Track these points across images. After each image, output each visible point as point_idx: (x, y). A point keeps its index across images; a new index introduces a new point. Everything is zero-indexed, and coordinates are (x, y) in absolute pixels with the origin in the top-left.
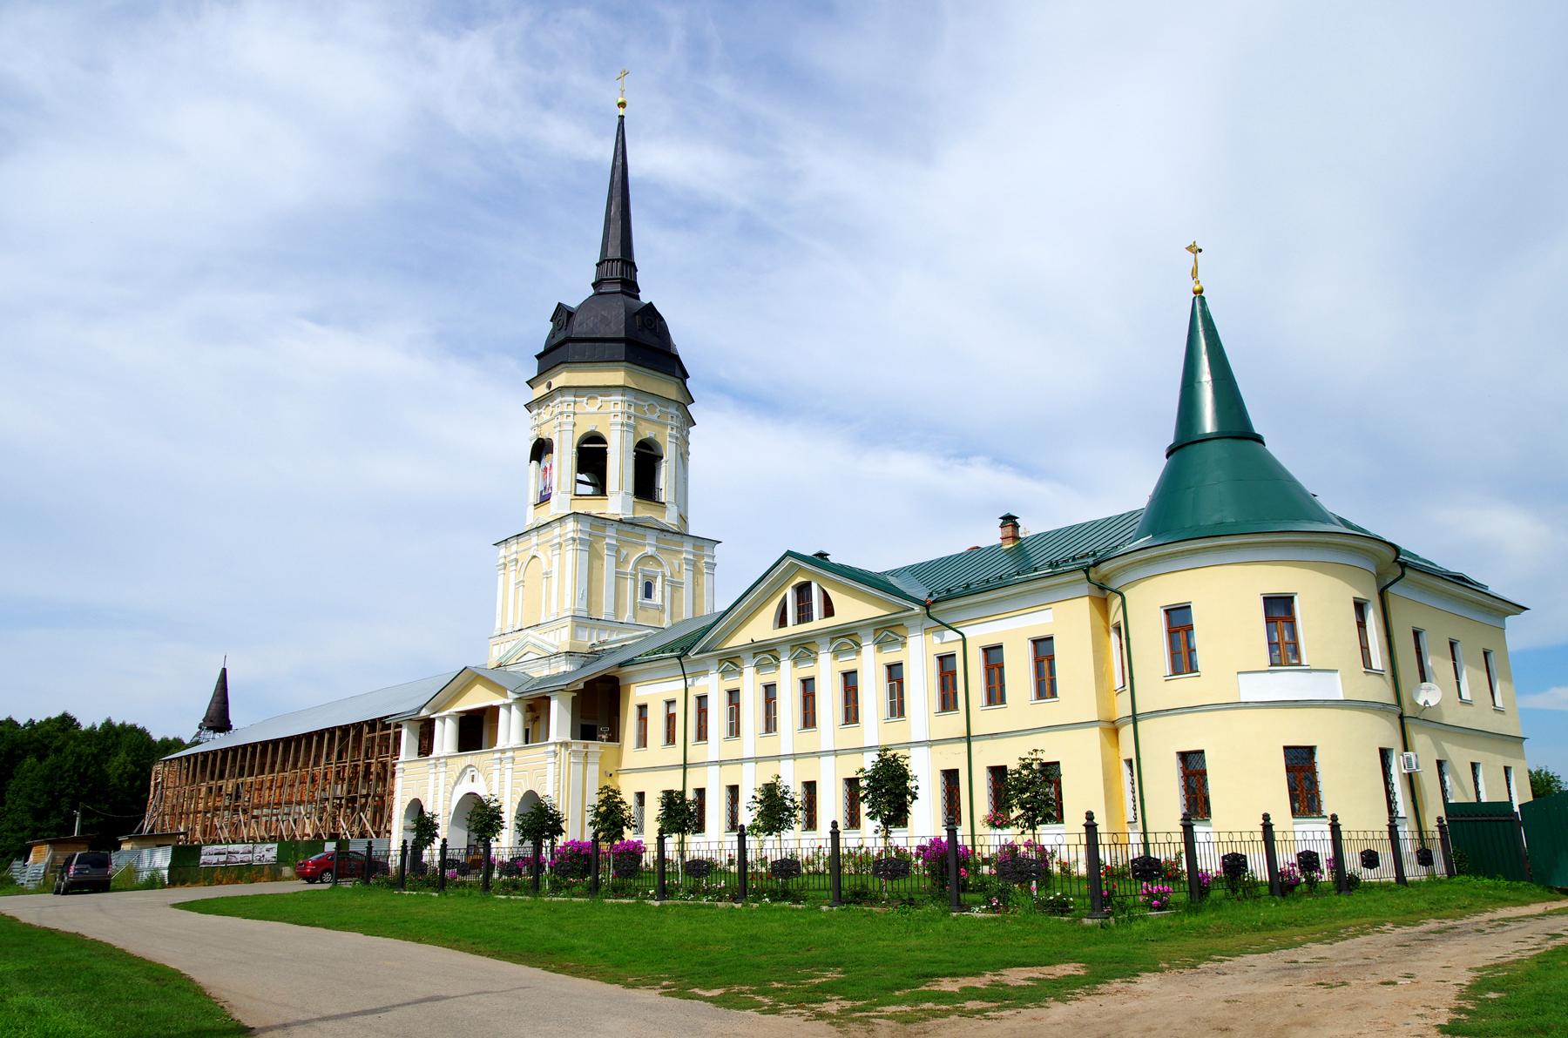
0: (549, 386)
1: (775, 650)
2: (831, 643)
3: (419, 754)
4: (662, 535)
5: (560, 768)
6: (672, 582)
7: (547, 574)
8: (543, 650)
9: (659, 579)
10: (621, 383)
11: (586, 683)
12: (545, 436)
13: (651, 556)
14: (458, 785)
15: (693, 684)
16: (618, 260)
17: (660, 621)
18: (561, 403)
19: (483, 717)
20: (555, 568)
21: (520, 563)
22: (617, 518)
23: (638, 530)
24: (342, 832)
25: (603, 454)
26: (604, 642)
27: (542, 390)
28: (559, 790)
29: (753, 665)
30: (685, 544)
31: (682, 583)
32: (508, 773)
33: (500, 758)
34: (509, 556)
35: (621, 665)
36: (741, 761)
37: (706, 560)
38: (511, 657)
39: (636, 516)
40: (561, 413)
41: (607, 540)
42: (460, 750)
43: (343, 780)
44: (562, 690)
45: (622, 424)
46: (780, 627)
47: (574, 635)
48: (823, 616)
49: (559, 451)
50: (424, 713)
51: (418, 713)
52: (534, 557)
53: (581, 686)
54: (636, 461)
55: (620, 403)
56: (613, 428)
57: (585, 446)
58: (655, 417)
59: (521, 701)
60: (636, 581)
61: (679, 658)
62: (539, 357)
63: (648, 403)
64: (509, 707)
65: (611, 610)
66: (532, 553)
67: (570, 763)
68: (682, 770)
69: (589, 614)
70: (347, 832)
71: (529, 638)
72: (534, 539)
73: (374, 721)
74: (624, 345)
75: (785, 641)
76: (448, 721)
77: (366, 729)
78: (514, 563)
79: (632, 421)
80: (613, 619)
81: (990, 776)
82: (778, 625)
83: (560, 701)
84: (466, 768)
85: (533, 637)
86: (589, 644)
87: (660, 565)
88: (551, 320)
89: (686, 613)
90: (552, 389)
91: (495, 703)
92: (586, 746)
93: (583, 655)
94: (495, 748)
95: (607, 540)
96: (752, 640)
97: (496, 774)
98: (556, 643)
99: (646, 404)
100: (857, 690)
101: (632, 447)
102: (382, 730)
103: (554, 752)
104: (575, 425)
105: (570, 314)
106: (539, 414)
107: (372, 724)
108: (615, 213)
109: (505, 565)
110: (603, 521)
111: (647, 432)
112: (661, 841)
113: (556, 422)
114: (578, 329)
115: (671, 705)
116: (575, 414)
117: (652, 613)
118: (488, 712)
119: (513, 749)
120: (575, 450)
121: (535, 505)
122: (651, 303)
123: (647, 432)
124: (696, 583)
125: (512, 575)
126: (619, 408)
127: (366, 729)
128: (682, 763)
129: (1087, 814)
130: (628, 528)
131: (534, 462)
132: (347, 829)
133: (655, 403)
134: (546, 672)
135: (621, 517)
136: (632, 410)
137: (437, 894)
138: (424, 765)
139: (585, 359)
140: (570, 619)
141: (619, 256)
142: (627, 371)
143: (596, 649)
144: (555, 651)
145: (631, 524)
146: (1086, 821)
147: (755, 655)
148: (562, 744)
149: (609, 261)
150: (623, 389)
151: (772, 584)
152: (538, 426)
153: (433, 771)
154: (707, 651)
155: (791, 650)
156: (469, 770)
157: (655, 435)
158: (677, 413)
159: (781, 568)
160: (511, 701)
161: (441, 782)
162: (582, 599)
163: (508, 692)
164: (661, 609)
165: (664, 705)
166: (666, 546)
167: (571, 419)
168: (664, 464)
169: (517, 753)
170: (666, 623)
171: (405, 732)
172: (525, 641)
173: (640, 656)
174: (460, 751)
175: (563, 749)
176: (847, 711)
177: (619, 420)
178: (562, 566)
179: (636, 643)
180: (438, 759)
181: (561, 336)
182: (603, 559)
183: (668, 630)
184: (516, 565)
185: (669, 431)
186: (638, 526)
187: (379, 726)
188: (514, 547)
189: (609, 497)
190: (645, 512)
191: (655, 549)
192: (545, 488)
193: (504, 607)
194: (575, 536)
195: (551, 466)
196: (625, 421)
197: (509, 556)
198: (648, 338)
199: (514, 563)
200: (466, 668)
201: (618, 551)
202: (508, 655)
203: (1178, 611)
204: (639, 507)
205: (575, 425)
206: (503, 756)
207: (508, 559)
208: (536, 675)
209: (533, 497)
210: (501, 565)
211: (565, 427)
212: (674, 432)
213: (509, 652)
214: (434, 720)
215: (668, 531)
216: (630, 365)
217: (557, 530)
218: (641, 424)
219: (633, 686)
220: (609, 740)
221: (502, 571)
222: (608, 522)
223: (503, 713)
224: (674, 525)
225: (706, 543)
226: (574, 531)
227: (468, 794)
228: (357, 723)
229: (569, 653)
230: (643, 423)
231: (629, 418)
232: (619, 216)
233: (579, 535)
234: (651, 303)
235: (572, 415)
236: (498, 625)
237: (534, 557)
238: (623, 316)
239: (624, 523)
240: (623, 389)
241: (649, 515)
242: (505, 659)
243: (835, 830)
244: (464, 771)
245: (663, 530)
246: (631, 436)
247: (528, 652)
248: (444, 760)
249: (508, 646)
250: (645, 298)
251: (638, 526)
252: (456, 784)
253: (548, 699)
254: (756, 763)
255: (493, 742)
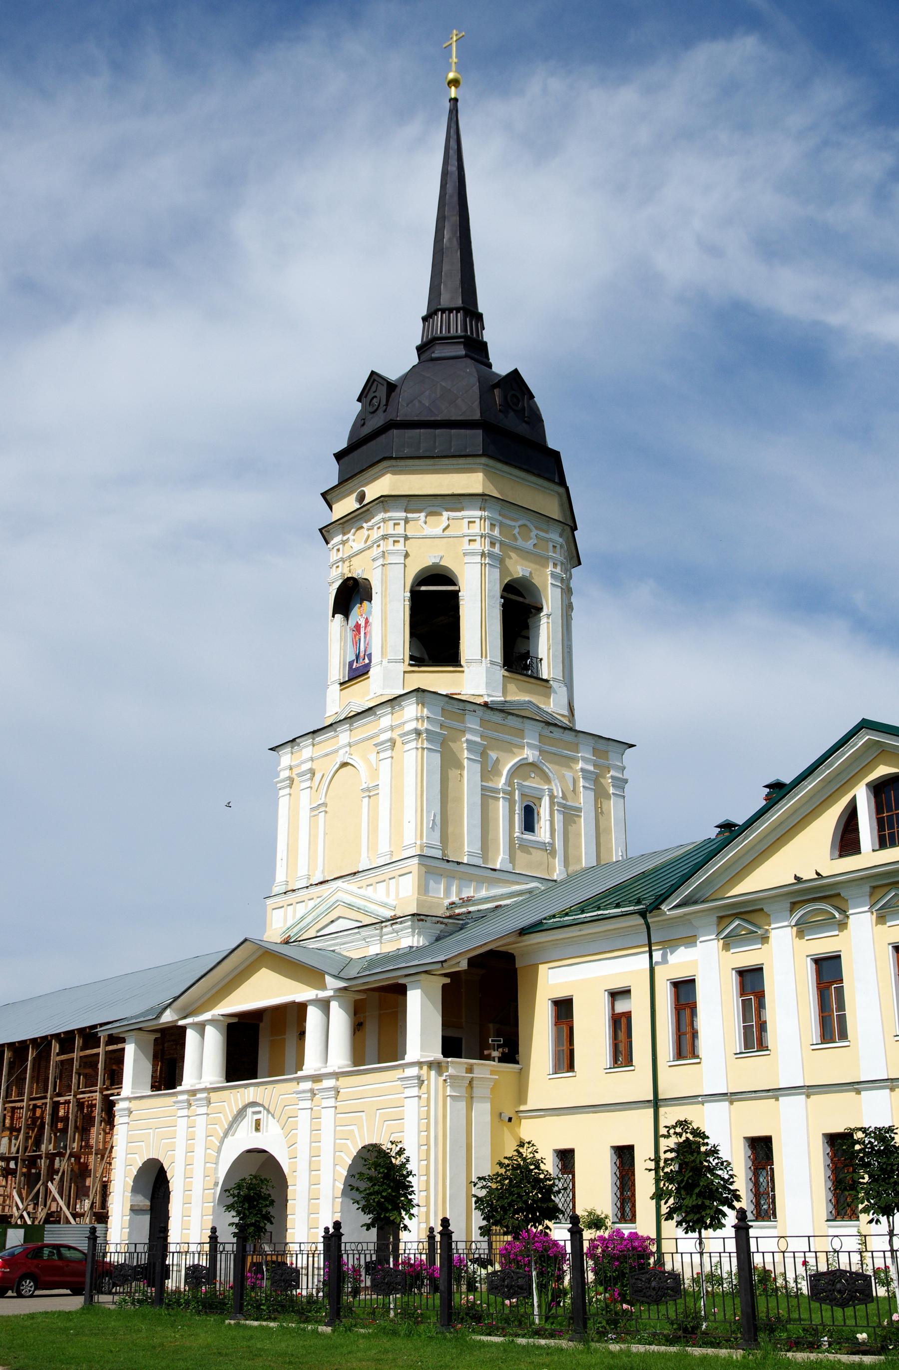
0: (361, 497)
1: (839, 895)
2: (792, 911)
3: (152, 1087)
4: (546, 731)
5: (428, 1105)
6: (565, 806)
7: (368, 790)
8: (366, 913)
9: (546, 801)
10: (478, 489)
11: (471, 961)
12: (357, 573)
13: (532, 764)
14: (230, 1138)
15: (665, 960)
16: (458, 310)
17: (549, 868)
18: (384, 521)
19: (258, 1025)
20: (384, 779)
21: (318, 776)
22: (480, 701)
23: (511, 721)
24: (16, 1214)
25: (453, 599)
26: (468, 901)
27: (347, 505)
28: (428, 1144)
29: (793, 923)
30: (581, 747)
31: (579, 810)
32: (328, 1116)
33: (312, 1091)
34: (298, 765)
35: (524, 932)
36: (775, 1093)
37: (612, 773)
38: (307, 928)
39: (508, 699)
40: (385, 537)
41: (469, 736)
42: (228, 1080)
43: (19, 1130)
44: (426, 972)
45: (483, 554)
46: (841, 856)
47: (423, 888)
48: (877, 847)
49: (384, 596)
50: (168, 1017)
51: (159, 1016)
52: (345, 765)
53: (464, 965)
54: (503, 611)
55: (478, 520)
56: (468, 559)
57: (423, 588)
58: (529, 545)
59: (347, 994)
60: (511, 803)
61: (643, 914)
62: (339, 456)
63: (520, 523)
64: (324, 1005)
65: (477, 848)
66: (340, 758)
67: (445, 1097)
68: (651, 1111)
69: (444, 854)
70: (25, 1214)
71: (341, 895)
72: (344, 736)
73: (70, 1035)
74: (480, 432)
75: (862, 879)
76: (210, 1030)
77: (55, 1047)
78: (308, 776)
79: (497, 550)
80: (479, 862)
81: (750, 1153)
82: (837, 853)
83: (425, 993)
84: (245, 1107)
85: (351, 893)
86: (446, 902)
87: (547, 780)
88: (359, 400)
89: (585, 858)
90: (366, 502)
91: (300, 998)
92: (470, 1070)
93: (440, 920)
94: (300, 1074)
95: (469, 736)
96: (796, 877)
97: (304, 1118)
98: (392, 901)
99: (517, 524)
100: (764, 996)
101: (497, 590)
102: (107, 1044)
103: (419, 1077)
104: (407, 555)
105: (391, 387)
106: (344, 543)
107: (66, 1040)
108: (450, 239)
109: (393, 742)
110: (461, 705)
111: (519, 568)
112: (445, 1237)
113: (375, 552)
114: (404, 410)
115: (618, 997)
116: (406, 538)
117: (538, 855)
118: (267, 1020)
119: (336, 1075)
120: (408, 594)
121: (341, 684)
122: (516, 372)
123: (519, 569)
124: (599, 813)
125: (305, 797)
126: (476, 529)
127: (55, 1047)
128: (651, 1097)
129: (325, 1228)
130: (497, 718)
131: (339, 617)
132: (26, 1209)
133: (528, 523)
134: (374, 949)
135: (486, 699)
136: (496, 532)
137: (329, 1329)
138: (164, 1102)
139: (421, 452)
140: (416, 861)
141: (459, 303)
142: (487, 475)
143: (457, 911)
144: (389, 914)
145: (502, 711)
146: (324, 1234)
147: (794, 906)
148: (431, 1065)
149: (443, 311)
150: (481, 499)
151: (827, 782)
152: (343, 560)
153: (185, 1112)
154: (695, 902)
155: (871, 895)
156: (250, 1110)
157: (531, 573)
158: (561, 540)
159: (848, 751)
160: (330, 993)
161: (200, 1131)
162: (433, 828)
163: (327, 978)
164: (549, 849)
165: (606, 998)
166: (553, 749)
167: (400, 546)
168: (544, 621)
169: (343, 1081)
170: (558, 873)
171: (130, 1050)
172: (333, 900)
173: (554, 916)
174: (228, 1080)
175: (433, 1073)
176: (747, 1031)
177: (477, 546)
178: (397, 776)
179: (516, 903)
180: (193, 1093)
181: (377, 421)
182: (460, 766)
183: (563, 882)
184: (312, 779)
185: (551, 568)
186: (513, 714)
187: (78, 1042)
188: (306, 751)
189: (465, 669)
190: (518, 695)
191: (538, 753)
192: (358, 657)
193: (292, 849)
194: (419, 727)
195: (367, 621)
196: (487, 549)
197: (298, 765)
198: (511, 422)
199: (308, 776)
200: (246, 940)
201: (484, 754)
202: (302, 925)
203: (829, 962)
204: (512, 687)
205: (407, 555)
206: (317, 1086)
207: (296, 771)
208: (355, 955)
209: (336, 671)
210: (283, 781)
211: (391, 559)
212: (558, 570)
213: (302, 918)
214: (183, 1029)
215: (555, 725)
216: (491, 462)
217: (386, 720)
218: (510, 558)
219: (542, 968)
220: (501, 1060)
221: (287, 791)
222: (469, 707)
223: (313, 1016)
224: (563, 716)
225: (612, 747)
226: (417, 719)
227: (249, 1151)
228: (41, 1038)
229: (418, 917)
230: (513, 555)
231: (493, 544)
232: (456, 243)
233: (426, 725)
234: (516, 372)
235: (402, 540)
236: (281, 875)
237: (345, 765)
238: (476, 389)
239: (492, 709)
240: (481, 499)
241: (527, 699)
242: (295, 930)
243: (213, 1235)
244: (240, 1114)
245: (548, 724)
246: (497, 572)
247: (339, 917)
248: (204, 1095)
249: (301, 910)
250: (501, 366)
251: (513, 714)
252: (226, 1134)
253: (401, 990)
254: (808, 1096)
255: (300, 1065)
